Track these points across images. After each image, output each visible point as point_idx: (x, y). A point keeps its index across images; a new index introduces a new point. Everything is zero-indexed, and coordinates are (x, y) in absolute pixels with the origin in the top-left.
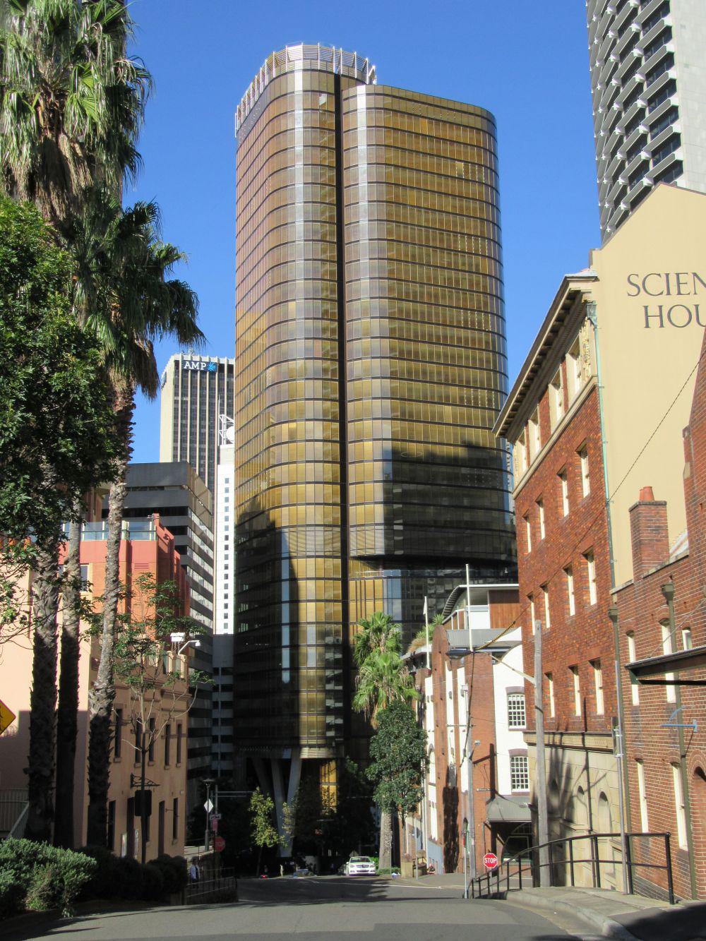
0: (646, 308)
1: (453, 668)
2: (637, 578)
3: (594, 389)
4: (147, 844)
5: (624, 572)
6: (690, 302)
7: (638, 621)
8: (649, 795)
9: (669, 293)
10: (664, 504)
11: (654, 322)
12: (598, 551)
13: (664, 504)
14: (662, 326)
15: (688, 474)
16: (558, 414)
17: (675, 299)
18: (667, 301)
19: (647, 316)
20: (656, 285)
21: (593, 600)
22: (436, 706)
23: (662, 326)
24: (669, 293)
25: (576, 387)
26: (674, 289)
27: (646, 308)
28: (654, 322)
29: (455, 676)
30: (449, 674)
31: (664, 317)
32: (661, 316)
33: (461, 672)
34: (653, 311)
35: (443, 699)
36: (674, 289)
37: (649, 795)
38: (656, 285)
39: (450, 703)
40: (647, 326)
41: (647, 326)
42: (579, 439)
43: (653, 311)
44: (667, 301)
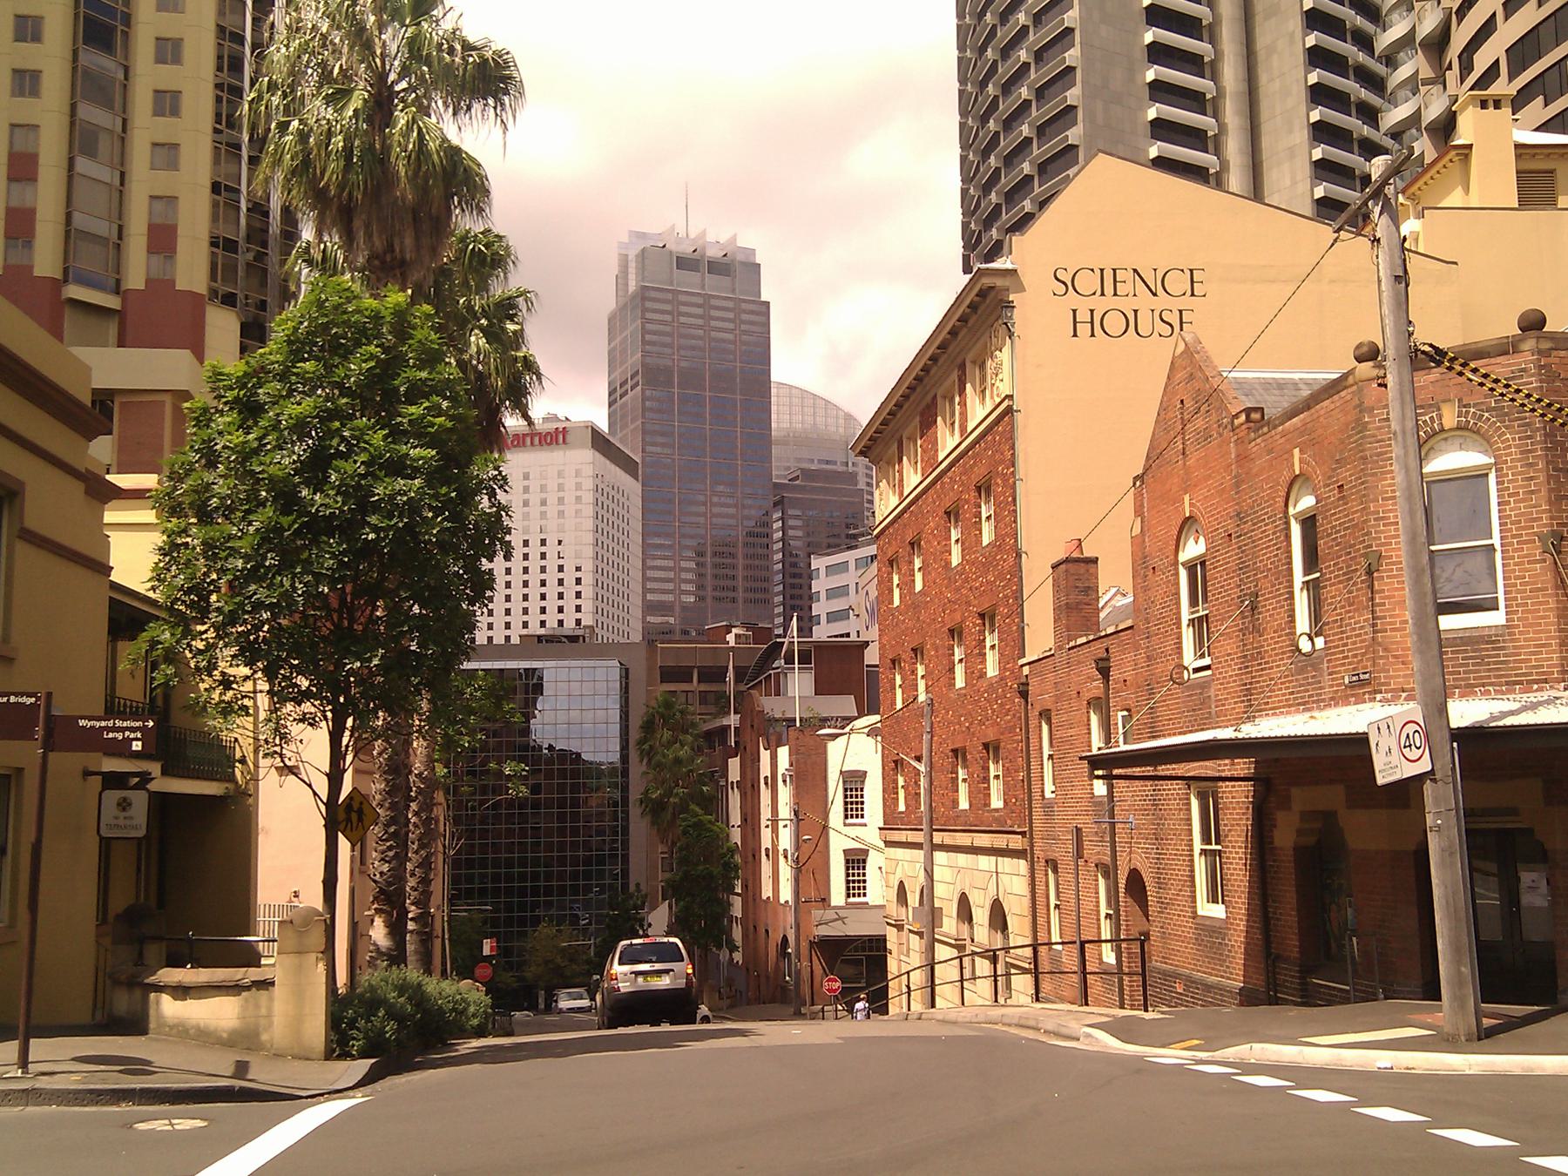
0: (1074, 311)
1: (773, 749)
2: (1060, 648)
3: (1009, 411)
4: (81, 487)
5: (1040, 635)
6: (1127, 305)
7: (1058, 699)
8: (761, 557)
9: (1103, 294)
10: (1095, 561)
11: (1084, 329)
12: (1001, 612)
13: (1095, 561)
14: (1093, 335)
15: (1137, 530)
16: (948, 441)
17: (1109, 301)
18: (1100, 304)
19: (1075, 323)
20: (1087, 282)
21: (992, 670)
22: (743, 796)
23: (1093, 335)
24: (1103, 294)
25: (978, 411)
26: (1109, 289)
27: (1074, 311)
28: (1084, 329)
29: (774, 758)
30: (765, 755)
31: (1096, 324)
32: (1092, 323)
33: (783, 753)
34: (1083, 316)
35: (755, 788)
36: (1109, 289)
37: (761, 557)
38: (1087, 282)
39: (765, 794)
40: (1075, 335)
41: (1075, 335)
42: (979, 472)
43: (1083, 316)
44: (1100, 304)
